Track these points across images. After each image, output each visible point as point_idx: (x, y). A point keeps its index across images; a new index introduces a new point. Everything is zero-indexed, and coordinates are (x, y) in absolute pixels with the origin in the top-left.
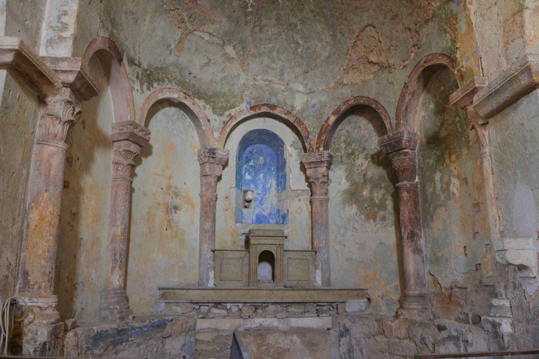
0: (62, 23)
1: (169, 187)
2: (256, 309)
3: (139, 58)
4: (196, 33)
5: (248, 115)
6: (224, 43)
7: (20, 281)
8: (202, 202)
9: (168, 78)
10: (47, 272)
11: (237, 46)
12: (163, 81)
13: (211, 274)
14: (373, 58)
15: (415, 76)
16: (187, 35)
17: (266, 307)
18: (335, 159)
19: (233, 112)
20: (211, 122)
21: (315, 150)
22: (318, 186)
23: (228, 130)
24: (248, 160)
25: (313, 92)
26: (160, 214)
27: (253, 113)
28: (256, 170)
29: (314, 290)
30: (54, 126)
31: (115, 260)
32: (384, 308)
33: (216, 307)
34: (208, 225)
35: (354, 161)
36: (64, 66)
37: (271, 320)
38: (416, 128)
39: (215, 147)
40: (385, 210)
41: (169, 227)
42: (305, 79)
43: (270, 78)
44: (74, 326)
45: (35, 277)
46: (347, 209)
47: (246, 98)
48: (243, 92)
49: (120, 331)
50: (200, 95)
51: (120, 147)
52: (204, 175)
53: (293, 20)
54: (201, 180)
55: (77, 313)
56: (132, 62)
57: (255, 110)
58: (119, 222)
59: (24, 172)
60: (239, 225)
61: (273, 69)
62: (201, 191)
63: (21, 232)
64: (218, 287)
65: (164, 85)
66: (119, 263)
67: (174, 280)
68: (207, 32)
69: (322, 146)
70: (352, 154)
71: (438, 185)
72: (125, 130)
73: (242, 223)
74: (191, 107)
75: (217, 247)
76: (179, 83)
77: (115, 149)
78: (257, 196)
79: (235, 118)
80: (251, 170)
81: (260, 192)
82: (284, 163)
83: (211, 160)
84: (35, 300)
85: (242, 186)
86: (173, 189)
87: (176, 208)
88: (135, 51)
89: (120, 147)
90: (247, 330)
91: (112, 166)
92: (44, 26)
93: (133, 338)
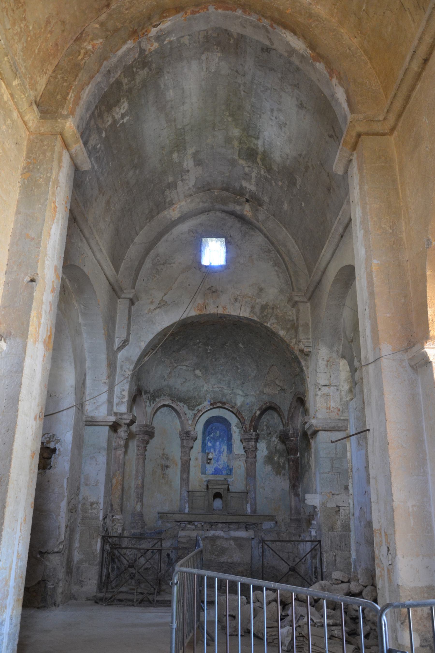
0: (122, 395)
2: (212, 526)
4: (178, 367)
8: (182, 462)
9: (163, 394)
12: (161, 396)
13: (187, 505)
14: (277, 382)
15: (295, 400)
17: (217, 525)
18: (260, 436)
19: (200, 407)
21: (248, 431)
22: (250, 453)
23: (197, 418)
24: (210, 434)
25: (248, 395)
27: (212, 407)
28: (215, 440)
29: (244, 515)
32: (283, 527)
34: (185, 476)
35: (271, 438)
36: (125, 417)
37: (220, 532)
38: (299, 425)
39: (190, 430)
40: (285, 470)
41: (164, 478)
42: (242, 387)
43: (222, 387)
46: (266, 467)
47: (208, 399)
48: (206, 395)
49: (142, 534)
50: (180, 400)
51: (140, 438)
52: (182, 447)
53: (234, 356)
57: (213, 406)
60: (203, 475)
61: (224, 381)
62: (181, 456)
64: (190, 513)
65: (161, 398)
67: (166, 508)
69: (252, 429)
70: (270, 434)
71: (306, 460)
72: (143, 429)
73: (206, 474)
75: (190, 489)
77: (137, 438)
78: (215, 457)
79: (201, 411)
81: (217, 454)
82: (231, 436)
83: (187, 438)
86: (165, 456)
90: (206, 537)
91: (136, 448)
92: (115, 397)
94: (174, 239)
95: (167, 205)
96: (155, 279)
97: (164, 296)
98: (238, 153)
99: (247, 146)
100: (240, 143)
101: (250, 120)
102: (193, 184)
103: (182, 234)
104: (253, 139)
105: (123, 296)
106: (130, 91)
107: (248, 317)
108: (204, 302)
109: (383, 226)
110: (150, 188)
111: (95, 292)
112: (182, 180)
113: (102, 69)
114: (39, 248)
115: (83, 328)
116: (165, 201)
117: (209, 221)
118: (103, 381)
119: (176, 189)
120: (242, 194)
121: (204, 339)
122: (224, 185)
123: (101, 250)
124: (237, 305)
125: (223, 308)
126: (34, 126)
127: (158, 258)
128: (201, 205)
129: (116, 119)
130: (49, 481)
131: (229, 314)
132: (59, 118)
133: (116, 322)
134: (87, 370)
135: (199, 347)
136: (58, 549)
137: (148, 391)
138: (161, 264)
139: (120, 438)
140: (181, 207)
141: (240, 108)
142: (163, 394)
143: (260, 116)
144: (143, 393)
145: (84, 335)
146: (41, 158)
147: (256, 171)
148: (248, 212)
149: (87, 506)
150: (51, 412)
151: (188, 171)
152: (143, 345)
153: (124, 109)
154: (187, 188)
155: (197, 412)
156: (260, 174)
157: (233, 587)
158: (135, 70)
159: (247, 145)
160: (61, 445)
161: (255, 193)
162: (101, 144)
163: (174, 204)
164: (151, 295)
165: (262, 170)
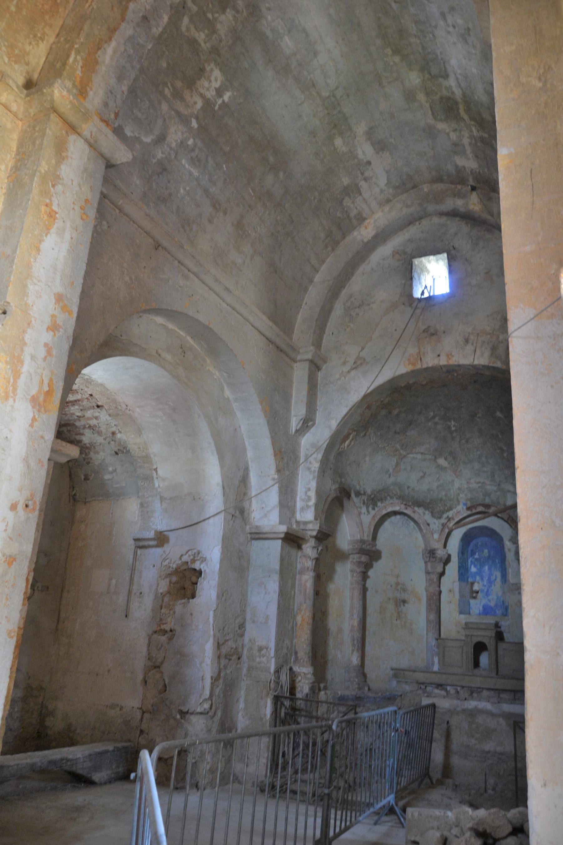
1: (398, 584)
2: (472, 693)
3: (364, 488)
5: (465, 515)
6: (436, 458)
7: (293, 657)
8: (427, 595)
9: (389, 495)
10: (307, 652)
11: (448, 457)
12: (386, 499)
13: (436, 660)
16: (402, 459)
17: (482, 692)
19: (450, 514)
20: (431, 526)
24: (473, 553)
26: (391, 607)
27: (469, 513)
30: (307, 562)
31: (353, 645)
33: (437, 688)
36: (310, 526)
39: (435, 547)
41: (399, 617)
43: (482, 480)
44: (325, 688)
45: (301, 655)
47: (462, 501)
50: (419, 503)
51: (354, 559)
52: (427, 573)
54: (426, 576)
55: (329, 681)
56: (358, 494)
57: (472, 510)
58: (355, 616)
59: (293, 593)
63: (293, 628)
65: (387, 502)
66: (356, 647)
67: (405, 663)
68: (420, 453)
74: (412, 515)
76: (399, 498)
77: (351, 560)
78: (483, 588)
79: (453, 519)
80: (476, 563)
83: (432, 559)
84: (301, 668)
85: (468, 578)
86: (400, 586)
87: (404, 602)
88: (360, 486)
89: (354, 559)
92: (298, 499)
93: (368, 705)
94: (372, 269)
95: (355, 222)
96: (348, 330)
97: (361, 351)
98: (430, 113)
99: (438, 96)
100: (427, 94)
101: (424, 48)
102: (386, 182)
103: (383, 259)
104: (441, 80)
105: (299, 357)
106: (215, 50)
107: (487, 364)
108: (418, 351)
109: (523, 80)
110: (314, 199)
111: (232, 350)
112: (366, 179)
113: (130, 15)
114: (12, 267)
115: (235, 405)
116: (348, 216)
117: (422, 232)
118: (271, 477)
119: (361, 194)
120: (462, 181)
121: (439, 410)
122: (434, 173)
123: (227, 289)
124: (469, 348)
125: (448, 355)
126: (22, 109)
127: (352, 299)
128: (405, 211)
129: (209, 99)
130: (191, 614)
131: (456, 363)
132: (45, 88)
133: (292, 396)
134: (250, 463)
135: (436, 423)
136: (202, 709)
137: (362, 492)
138: (356, 308)
139: (306, 556)
140: (375, 221)
141: (402, 33)
142: (389, 495)
143: (433, 35)
144: (353, 495)
145: (239, 414)
146: (30, 149)
147: (466, 134)
148: (475, 205)
149: (254, 652)
150: (196, 522)
151: (369, 163)
152: (334, 424)
153: (216, 80)
154: (377, 190)
155: (446, 521)
156: (474, 136)
157: (506, 792)
158: (210, 16)
159: (437, 94)
160: (207, 565)
161: (479, 172)
162: (194, 139)
163: (365, 219)
164: (343, 353)
165: (474, 129)
